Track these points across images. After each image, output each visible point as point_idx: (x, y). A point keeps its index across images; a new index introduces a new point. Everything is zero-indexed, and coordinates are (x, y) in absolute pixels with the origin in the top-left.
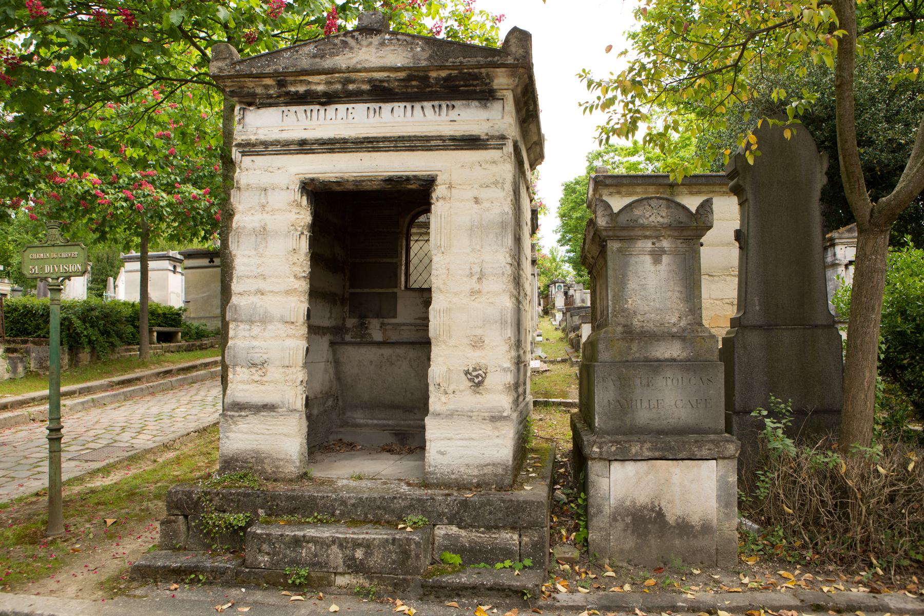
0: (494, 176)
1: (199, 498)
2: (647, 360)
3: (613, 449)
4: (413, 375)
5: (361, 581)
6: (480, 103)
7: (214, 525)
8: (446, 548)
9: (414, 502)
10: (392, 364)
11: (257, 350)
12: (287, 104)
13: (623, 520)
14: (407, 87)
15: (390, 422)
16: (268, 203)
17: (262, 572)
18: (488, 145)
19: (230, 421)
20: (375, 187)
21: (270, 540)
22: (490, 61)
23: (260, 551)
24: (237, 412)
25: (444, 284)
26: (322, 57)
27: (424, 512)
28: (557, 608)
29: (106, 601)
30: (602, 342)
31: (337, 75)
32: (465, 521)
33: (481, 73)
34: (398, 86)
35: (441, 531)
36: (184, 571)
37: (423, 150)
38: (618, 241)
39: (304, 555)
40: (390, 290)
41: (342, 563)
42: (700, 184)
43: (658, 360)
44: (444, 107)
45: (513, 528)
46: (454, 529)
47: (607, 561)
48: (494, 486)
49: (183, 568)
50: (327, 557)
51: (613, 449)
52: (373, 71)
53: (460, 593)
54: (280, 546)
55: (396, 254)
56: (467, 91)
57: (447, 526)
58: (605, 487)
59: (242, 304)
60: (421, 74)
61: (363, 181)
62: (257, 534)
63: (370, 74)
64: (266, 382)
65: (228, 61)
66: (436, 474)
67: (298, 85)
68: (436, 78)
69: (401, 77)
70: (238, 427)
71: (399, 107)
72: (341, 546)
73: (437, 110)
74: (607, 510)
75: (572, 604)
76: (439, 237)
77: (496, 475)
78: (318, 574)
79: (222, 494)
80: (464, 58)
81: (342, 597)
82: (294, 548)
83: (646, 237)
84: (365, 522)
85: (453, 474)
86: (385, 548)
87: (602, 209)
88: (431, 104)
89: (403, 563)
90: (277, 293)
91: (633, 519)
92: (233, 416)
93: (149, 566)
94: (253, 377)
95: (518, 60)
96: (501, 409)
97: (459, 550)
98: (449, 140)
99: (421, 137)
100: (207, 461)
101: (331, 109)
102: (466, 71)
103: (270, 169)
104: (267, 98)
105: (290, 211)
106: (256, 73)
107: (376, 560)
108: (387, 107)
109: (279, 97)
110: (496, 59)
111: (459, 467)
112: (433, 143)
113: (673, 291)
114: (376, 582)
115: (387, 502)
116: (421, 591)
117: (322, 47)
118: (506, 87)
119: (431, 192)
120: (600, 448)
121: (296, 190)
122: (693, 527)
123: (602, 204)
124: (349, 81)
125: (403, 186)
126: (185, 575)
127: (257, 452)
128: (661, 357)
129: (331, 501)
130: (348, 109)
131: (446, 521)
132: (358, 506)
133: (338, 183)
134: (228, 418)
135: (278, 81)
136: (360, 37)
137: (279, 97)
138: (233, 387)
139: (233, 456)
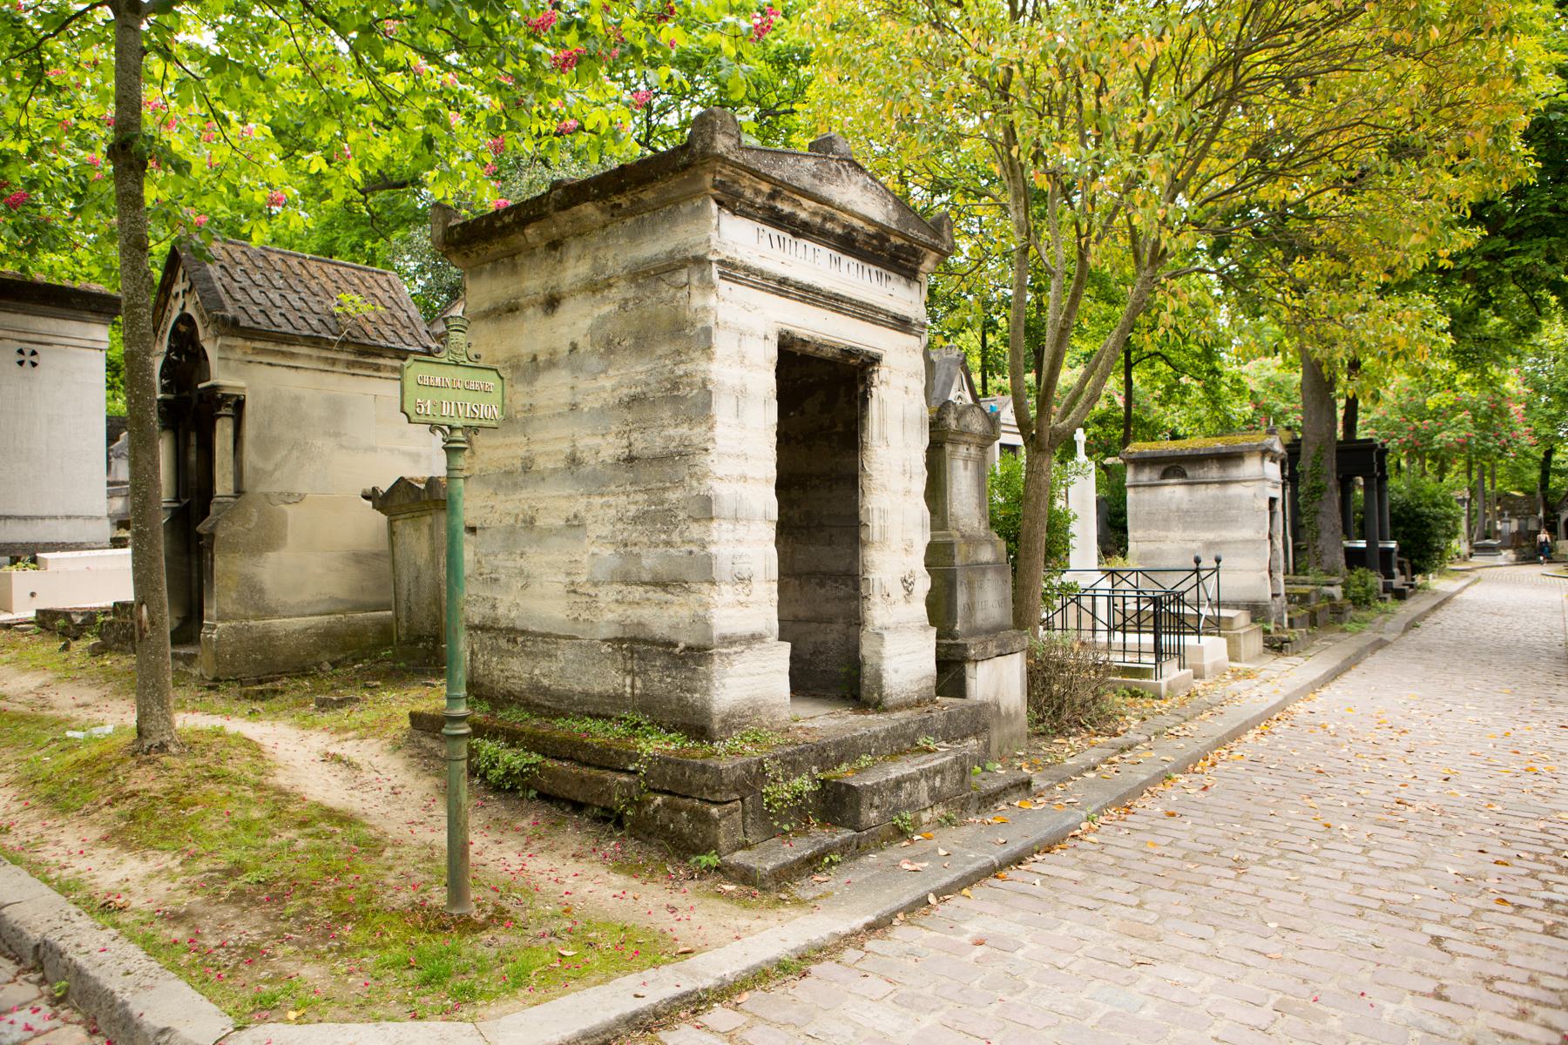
11: (745, 560)
12: (764, 221)
19: (727, 661)
31: (826, 208)
83: (965, 442)
89: (962, 781)
94: (739, 597)
104: (748, 205)
108: (846, 259)
109: (759, 208)
112: (881, 317)
124: (832, 219)
127: (753, 700)
134: (724, 658)
135: (775, 191)
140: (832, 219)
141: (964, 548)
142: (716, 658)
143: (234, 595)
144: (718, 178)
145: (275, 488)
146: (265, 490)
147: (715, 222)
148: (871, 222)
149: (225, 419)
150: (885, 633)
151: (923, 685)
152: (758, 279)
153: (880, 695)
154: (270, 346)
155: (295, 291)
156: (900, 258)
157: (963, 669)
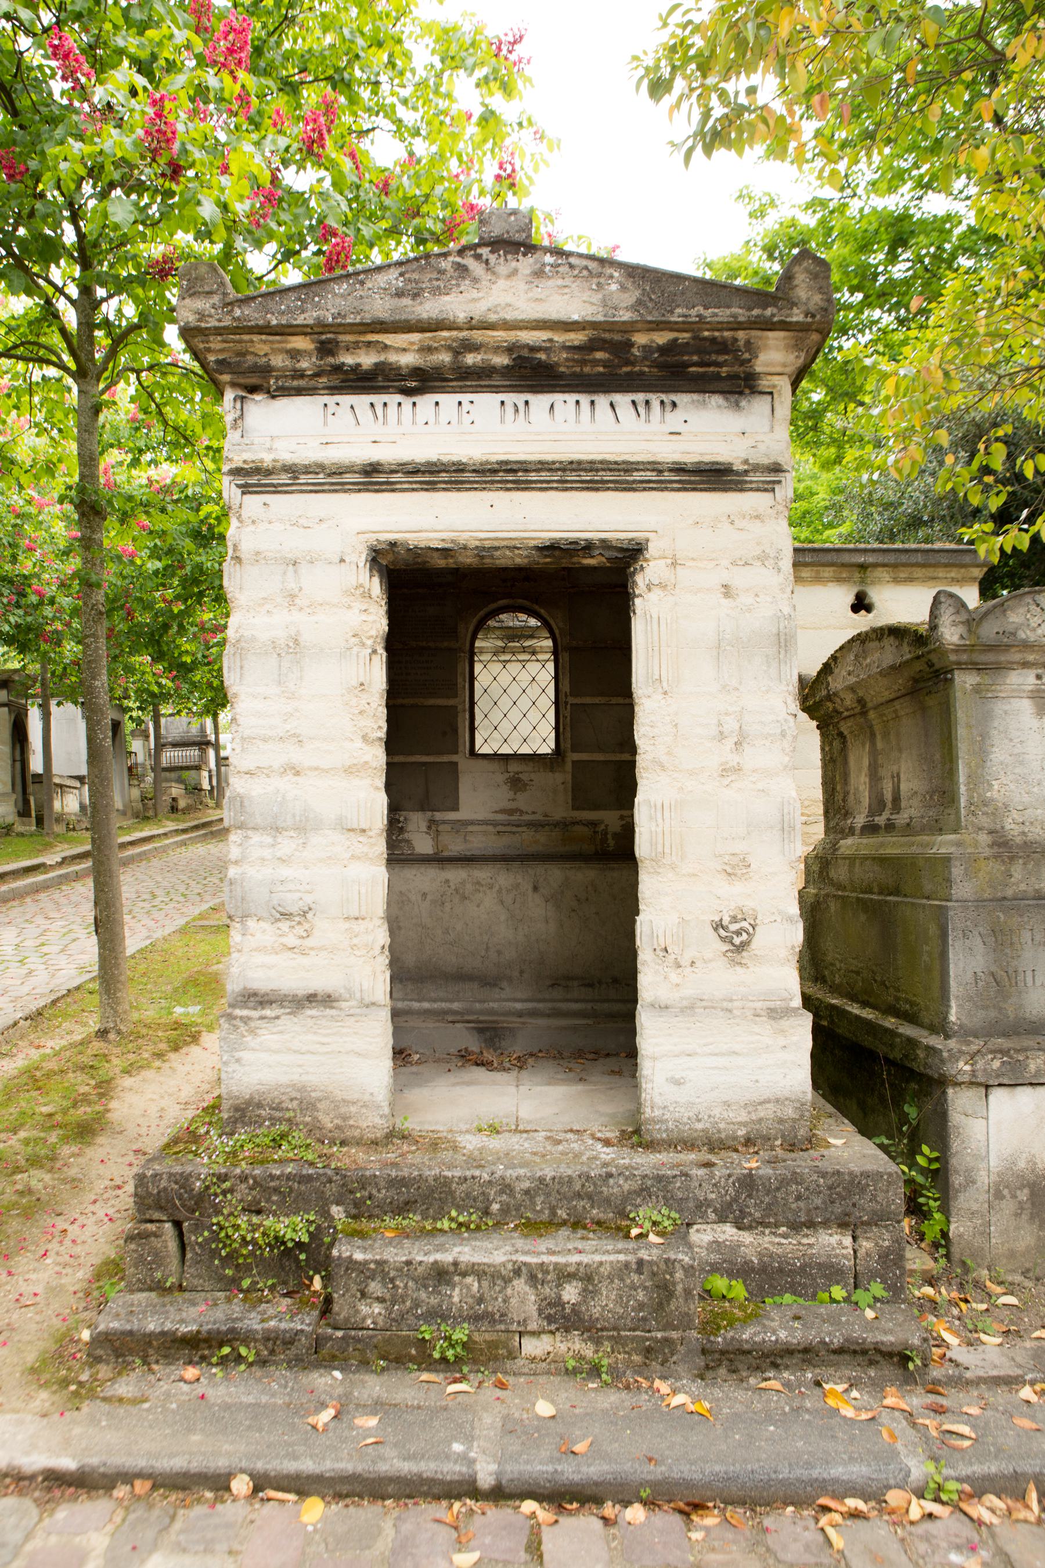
0: (758, 544)
1: (207, 1188)
3: (996, 1064)
4: (503, 918)
5: (577, 1347)
6: (727, 399)
7: (244, 1242)
8: (715, 1269)
9: (649, 1183)
10: (464, 898)
13: (1014, 1197)
14: (583, 362)
15: (456, 1006)
16: (301, 589)
17: (371, 1337)
18: (746, 482)
19: (243, 1029)
20: (518, 561)
21: (384, 1275)
22: (757, 317)
23: (364, 1295)
24: (255, 1009)
25: (669, 753)
26: (415, 296)
27: (670, 1201)
28: (969, 1383)
29: (67, 1414)
30: (958, 863)
31: (445, 334)
32: (750, 1214)
33: (736, 340)
34: (567, 360)
35: (703, 1235)
36: (206, 1341)
37: (616, 489)
38: (974, 672)
39: (456, 1299)
40: (445, 759)
41: (535, 1314)
42: (912, 565)
44: (656, 404)
45: (843, 1225)
46: (728, 1232)
47: (986, 1272)
48: (778, 1142)
49: (204, 1335)
50: (504, 1301)
51: (996, 1064)
52: (521, 329)
53: (779, 1361)
54: (406, 1286)
55: (452, 690)
56: (702, 377)
57: (715, 1226)
58: (979, 1137)
59: (254, 794)
60: (617, 337)
61: (497, 549)
62: (356, 1262)
63: (513, 333)
64: (312, 949)
65: (216, 299)
67: (362, 352)
68: (644, 347)
69: (577, 343)
70: (259, 1040)
71: (565, 402)
72: (533, 1279)
73: (642, 410)
74: (983, 1179)
75: (995, 1373)
76: (656, 661)
77: (781, 1121)
78: (488, 1337)
79: (254, 1178)
80: (706, 308)
81: (542, 1379)
82: (435, 1286)
83: (1025, 665)
84: (552, 1224)
85: (699, 1121)
86: (622, 1280)
87: (952, 610)
88: (628, 397)
90: (327, 771)
91: (1033, 1194)
92: (249, 1018)
93: (131, 1333)
94: (284, 940)
95: (813, 316)
96: (785, 995)
97: (741, 1271)
98: (671, 470)
99: (616, 463)
100: (93, 1082)
101: (426, 401)
102: (706, 334)
104: (293, 378)
105: (349, 607)
106: (277, 326)
108: (540, 402)
109: (317, 375)
110: (769, 312)
112: (637, 476)
114: (607, 1346)
115: (595, 1184)
116: (701, 1361)
117: (415, 276)
118: (779, 369)
119: (634, 573)
121: (361, 565)
123: (950, 601)
124: (470, 347)
125: (575, 560)
126: (210, 1347)
127: (302, 1089)
130: (460, 403)
131: (712, 1216)
132: (537, 1194)
133: (445, 552)
134: (238, 1022)
135: (322, 343)
136: (493, 258)
137: (317, 375)
138: (242, 960)
139: (252, 1098)
140: (470, 347)
151: (767, 1112)
157: (944, 1093)
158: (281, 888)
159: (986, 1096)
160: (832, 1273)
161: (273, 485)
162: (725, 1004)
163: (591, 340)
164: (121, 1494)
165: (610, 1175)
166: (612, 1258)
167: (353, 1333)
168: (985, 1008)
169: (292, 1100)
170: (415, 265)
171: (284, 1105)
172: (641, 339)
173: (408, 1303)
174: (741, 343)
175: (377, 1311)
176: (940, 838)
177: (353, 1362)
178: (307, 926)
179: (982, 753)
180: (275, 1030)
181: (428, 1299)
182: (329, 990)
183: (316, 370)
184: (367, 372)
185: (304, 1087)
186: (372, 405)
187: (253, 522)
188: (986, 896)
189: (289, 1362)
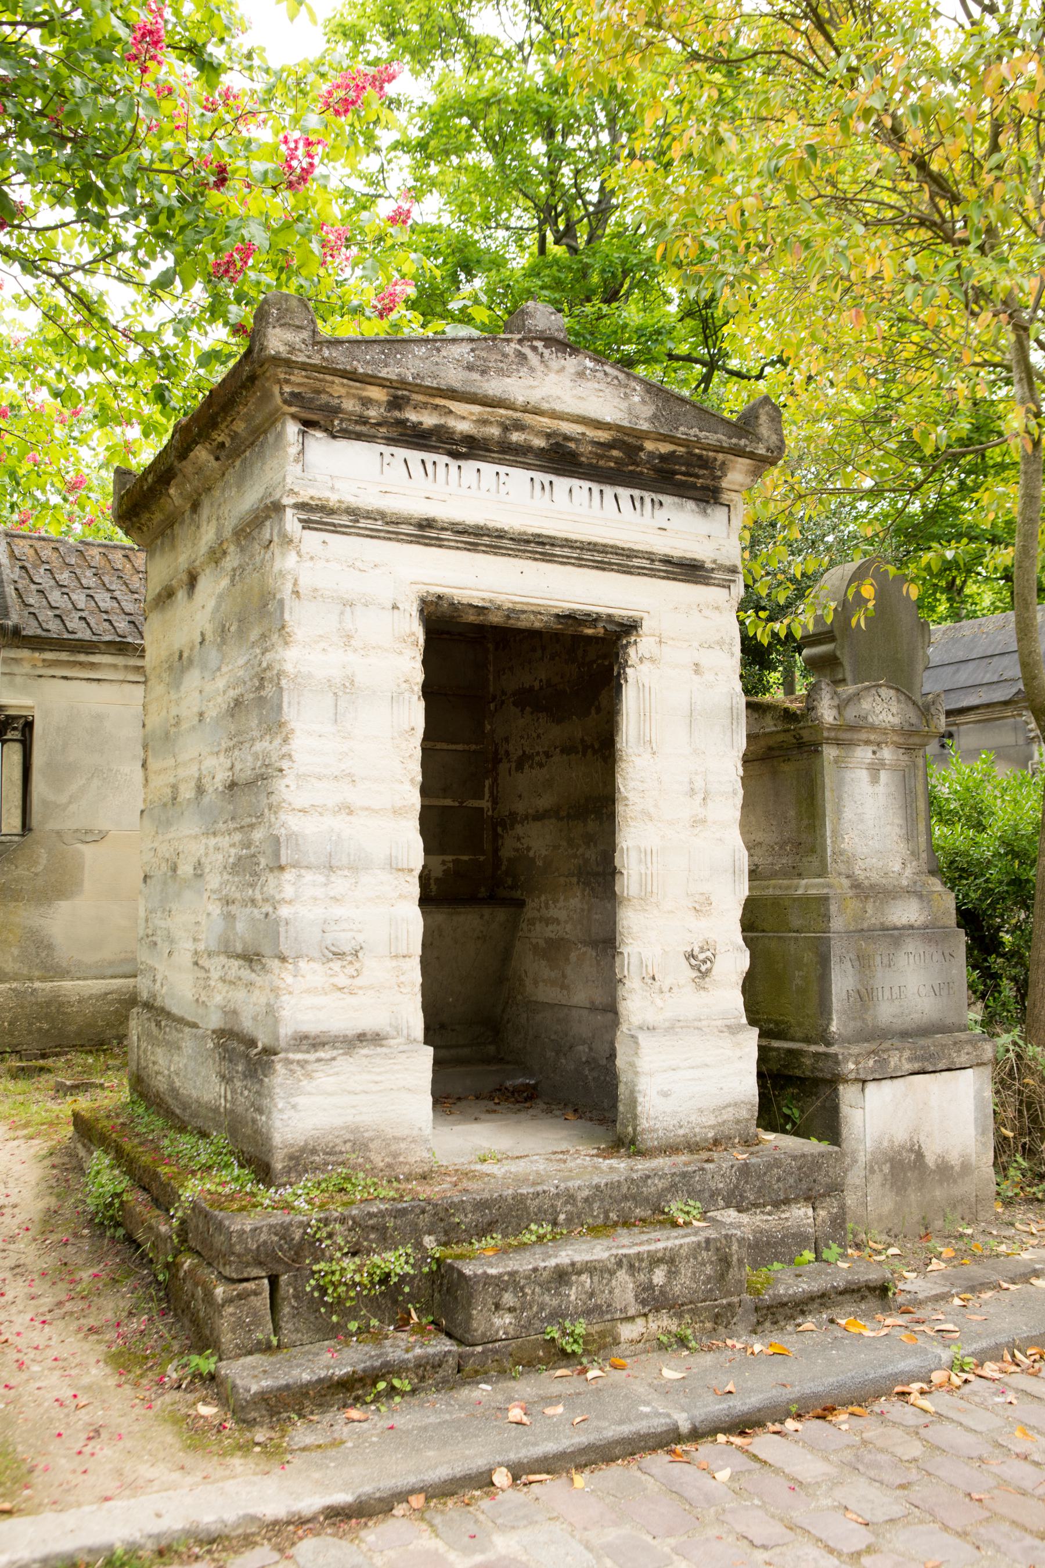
2: (884, 928)
3: (871, 1063)
5: (665, 1323)
12: (390, 441)
14: (601, 457)
19: (299, 1072)
21: (516, 1284)
25: (656, 806)
31: (502, 411)
33: (715, 459)
36: (361, 1380)
37: (618, 571)
39: (573, 1298)
41: (633, 1300)
43: (896, 928)
45: (807, 1199)
50: (610, 1292)
52: (562, 419)
54: (533, 1293)
59: (307, 832)
61: (524, 612)
64: (360, 988)
65: (305, 334)
66: (656, 1130)
70: (314, 1083)
71: (581, 486)
73: (638, 504)
74: (862, 1159)
79: (353, 1219)
81: (643, 1357)
83: (867, 742)
85: (681, 1127)
86: (695, 1258)
89: (722, 1277)
90: (376, 811)
91: (892, 1167)
92: (306, 1062)
93: (287, 1387)
94: (334, 980)
98: (660, 561)
99: (623, 549)
102: (697, 451)
103: (358, 564)
104: (356, 422)
105: (401, 653)
107: (684, 1283)
108: (562, 483)
109: (379, 424)
110: (743, 442)
111: (688, 1116)
112: (636, 562)
113: (892, 824)
117: (484, 354)
120: (857, 1063)
122: (952, 1167)
124: (519, 426)
128: (898, 924)
129: (551, 1199)
131: (722, 1203)
132: (594, 1201)
134: (294, 1067)
135: (396, 397)
136: (547, 352)
137: (379, 424)
139: (306, 1144)
140: (519, 426)
141: (853, 905)
142: (278, 1067)
143: (16, 951)
144: (287, 389)
145: (70, 824)
146: (58, 827)
147: (293, 450)
148: (598, 424)
149: (10, 744)
150: (641, 1037)
151: (728, 1115)
152: (379, 525)
153: (635, 1130)
154: (64, 656)
155: (108, 590)
156: (674, 473)
157: (836, 1090)
158: (336, 928)
159: (863, 1090)
160: (801, 1240)
161: (334, 525)
162: (696, 1024)
163: (614, 440)
164: (402, 1512)
165: (648, 1177)
166: (687, 1240)
167: (490, 1346)
168: (854, 1019)
169: (345, 1142)
170: (484, 344)
171: (337, 1149)
172: (649, 446)
173: (535, 1309)
174: (718, 463)
175: (507, 1321)
176: (804, 882)
177: (493, 1373)
178: (357, 965)
179: (839, 812)
180: (331, 1072)
181: (551, 1301)
182: (376, 1028)
183: (380, 419)
184: (424, 431)
185: (357, 1128)
186: (423, 461)
187: (312, 558)
188: (851, 928)
189: (436, 1386)
